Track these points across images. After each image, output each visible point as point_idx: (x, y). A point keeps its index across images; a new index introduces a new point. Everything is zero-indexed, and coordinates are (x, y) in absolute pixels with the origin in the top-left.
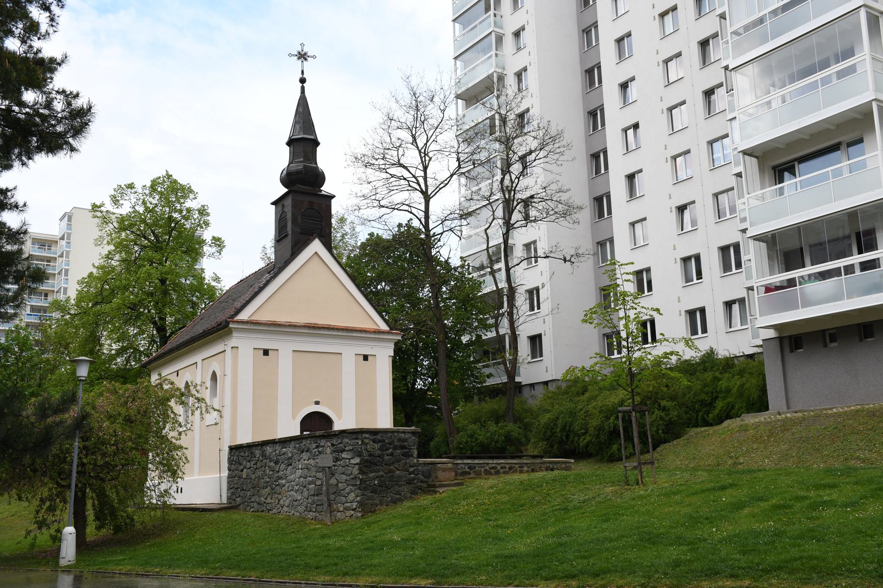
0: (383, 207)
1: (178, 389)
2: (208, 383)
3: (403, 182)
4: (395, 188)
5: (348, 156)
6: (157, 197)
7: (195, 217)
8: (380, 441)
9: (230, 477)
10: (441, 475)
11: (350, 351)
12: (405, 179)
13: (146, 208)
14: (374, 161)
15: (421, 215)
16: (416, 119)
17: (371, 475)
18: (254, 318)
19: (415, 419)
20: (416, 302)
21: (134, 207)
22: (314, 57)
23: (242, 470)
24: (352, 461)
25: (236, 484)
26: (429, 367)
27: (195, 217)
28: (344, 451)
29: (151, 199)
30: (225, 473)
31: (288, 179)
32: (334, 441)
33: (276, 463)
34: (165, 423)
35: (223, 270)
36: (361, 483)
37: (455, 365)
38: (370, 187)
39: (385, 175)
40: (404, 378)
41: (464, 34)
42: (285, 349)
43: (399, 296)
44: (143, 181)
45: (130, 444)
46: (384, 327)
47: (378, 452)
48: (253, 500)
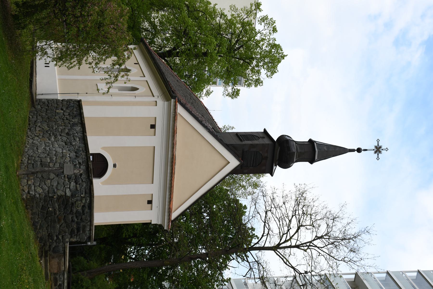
0: (266, 213)
1: (124, 62)
2: (129, 85)
3: (286, 229)
4: (281, 224)
5: (303, 186)
6: (267, 49)
7: (254, 77)
8: (83, 211)
9: (57, 100)
10: (55, 262)
11: (154, 189)
12: (288, 230)
13: (259, 42)
14: (301, 206)
15: (261, 244)
16: (336, 238)
17: (56, 205)
18: (179, 118)
19: (102, 246)
20: (194, 244)
21: (259, 32)
22: (378, 158)
23: (62, 109)
24: (68, 190)
25: (52, 105)
26: (143, 255)
27: (254, 77)
28: (76, 184)
29: (266, 45)
30: (60, 97)
31: (284, 141)
32: (84, 176)
33: (68, 134)
34: (99, 53)
35: (216, 99)
36: (50, 197)
37: (145, 276)
38: (281, 204)
39: (290, 214)
40: (135, 236)
41: (408, 280)
42: (156, 141)
43: (200, 229)
44: (279, 38)
45: (82, 26)
46: (174, 215)
47: (75, 210)
48: (39, 117)
